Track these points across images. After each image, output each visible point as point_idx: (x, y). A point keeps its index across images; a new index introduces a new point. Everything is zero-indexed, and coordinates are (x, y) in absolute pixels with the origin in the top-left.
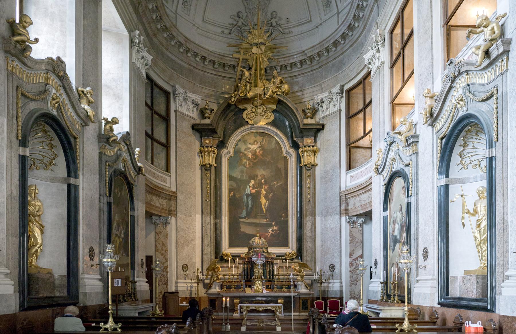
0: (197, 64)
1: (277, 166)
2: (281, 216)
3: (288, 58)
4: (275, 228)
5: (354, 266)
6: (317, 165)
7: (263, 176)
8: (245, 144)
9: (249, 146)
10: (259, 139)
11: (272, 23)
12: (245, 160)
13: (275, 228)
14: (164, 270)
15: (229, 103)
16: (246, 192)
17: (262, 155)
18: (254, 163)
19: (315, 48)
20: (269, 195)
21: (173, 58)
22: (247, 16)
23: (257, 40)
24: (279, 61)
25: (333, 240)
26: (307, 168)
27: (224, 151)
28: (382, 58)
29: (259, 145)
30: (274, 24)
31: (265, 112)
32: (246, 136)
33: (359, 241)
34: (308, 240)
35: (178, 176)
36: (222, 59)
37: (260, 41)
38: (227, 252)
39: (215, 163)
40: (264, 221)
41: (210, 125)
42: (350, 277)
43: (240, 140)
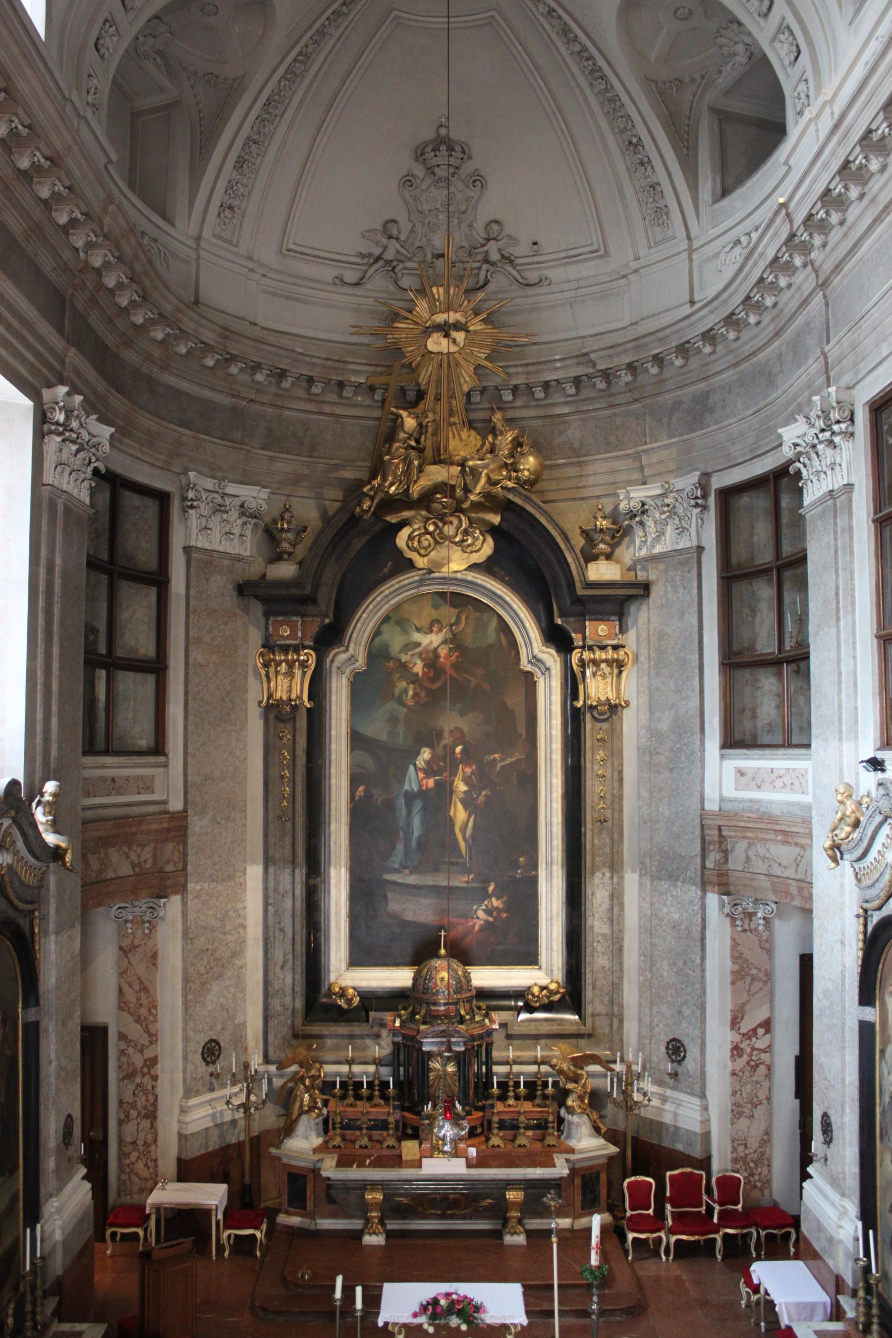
0: (258, 391)
2: (516, 866)
4: (495, 902)
5: (745, 1058)
6: (627, 704)
7: (458, 735)
8: (405, 631)
9: (417, 637)
10: (448, 613)
12: (403, 684)
13: (495, 902)
14: (145, 1070)
15: (353, 516)
16: (407, 787)
17: (456, 667)
18: (431, 693)
19: (620, 349)
23: (445, 316)
24: (508, 374)
25: (681, 964)
26: (595, 714)
27: (338, 657)
30: (495, 257)
31: (466, 532)
33: (761, 975)
36: (335, 368)
37: (453, 317)
39: (310, 699)
40: (460, 881)
42: (734, 1093)
43: (386, 619)
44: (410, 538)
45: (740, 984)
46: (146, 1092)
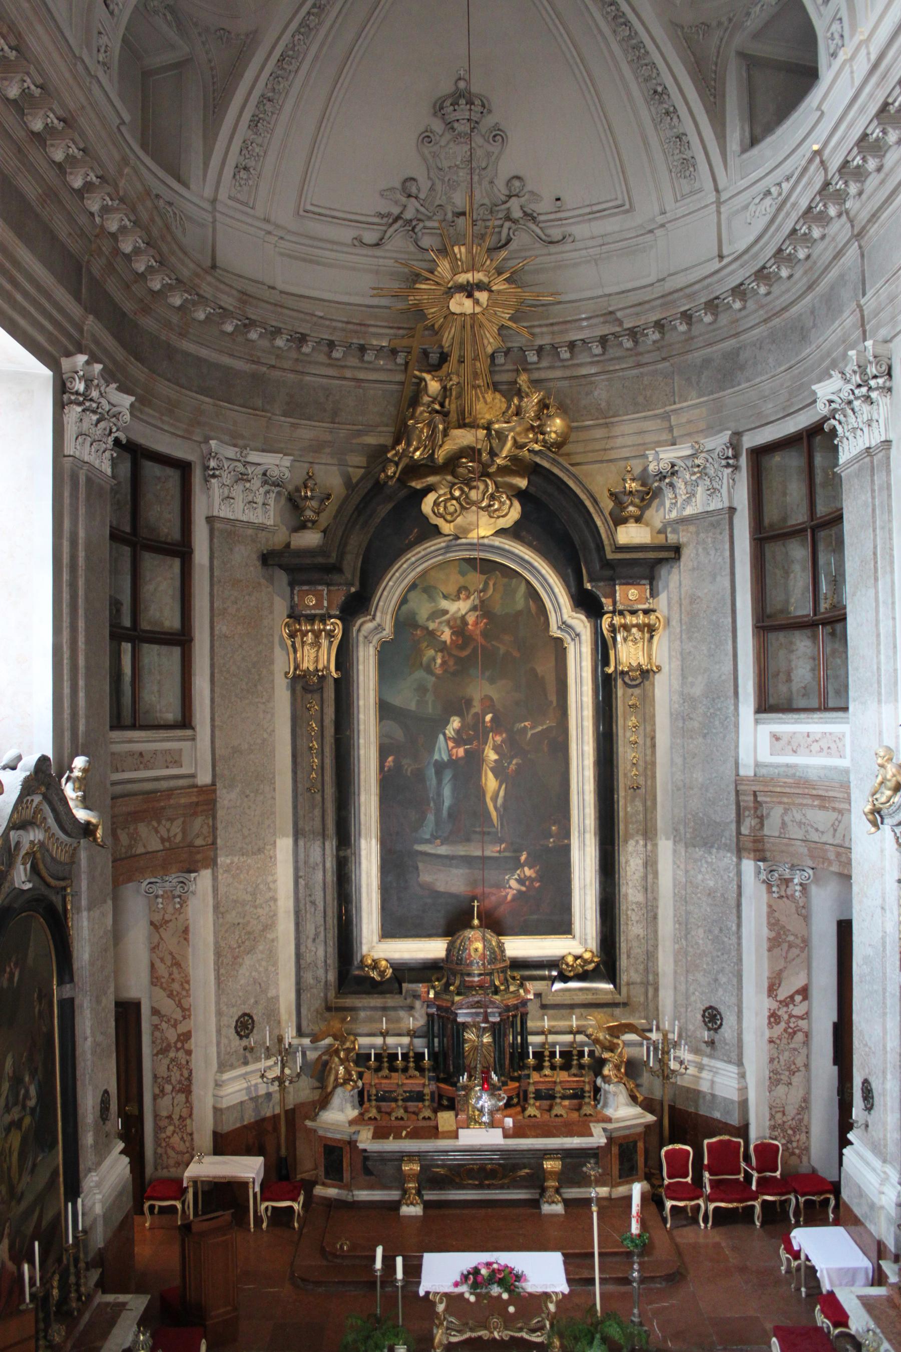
0: (278, 357)
1: (533, 670)
3: (563, 327)
4: (528, 872)
5: (783, 1025)
6: (659, 669)
8: (432, 598)
9: (444, 604)
10: (475, 579)
11: (508, 209)
12: (431, 652)
13: (528, 872)
14: (179, 1045)
16: (436, 757)
17: (485, 634)
18: (459, 661)
19: (647, 306)
20: (510, 763)
21: (204, 353)
22: (432, 189)
24: (533, 334)
25: (716, 932)
26: (627, 679)
27: (365, 626)
28: (882, 429)
29: (473, 600)
30: (517, 214)
31: (492, 497)
32: (432, 573)
34: (634, 917)
35: (217, 733)
36: (356, 332)
38: (376, 955)
39: (337, 669)
40: (492, 850)
41: (320, 551)
42: (772, 1060)
43: (413, 587)
44: (436, 503)
45: (776, 951)
46: (180, 1067)
